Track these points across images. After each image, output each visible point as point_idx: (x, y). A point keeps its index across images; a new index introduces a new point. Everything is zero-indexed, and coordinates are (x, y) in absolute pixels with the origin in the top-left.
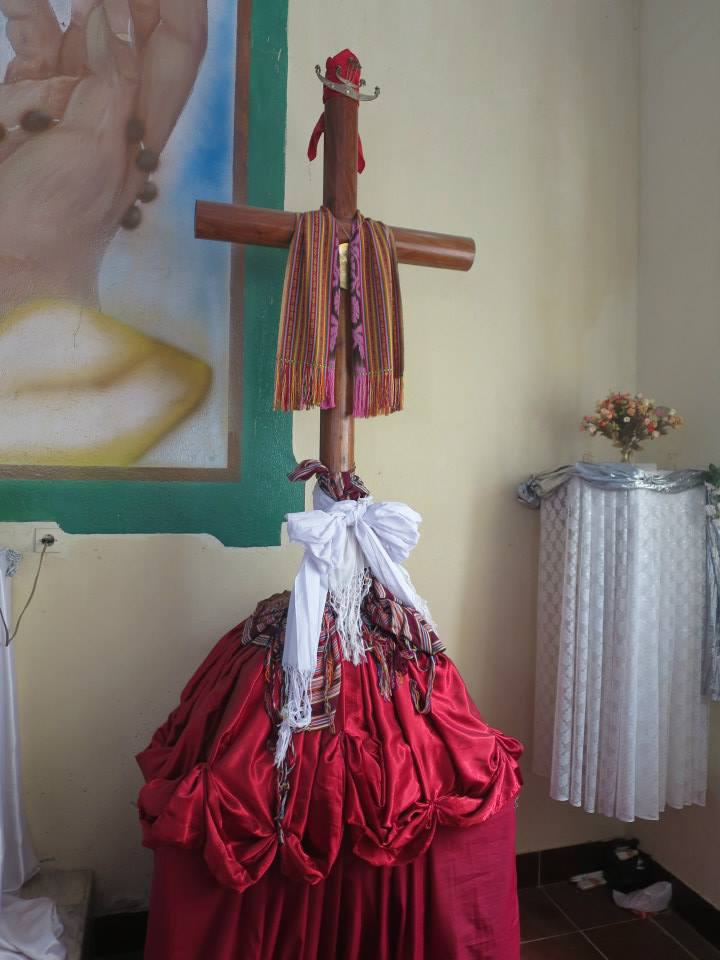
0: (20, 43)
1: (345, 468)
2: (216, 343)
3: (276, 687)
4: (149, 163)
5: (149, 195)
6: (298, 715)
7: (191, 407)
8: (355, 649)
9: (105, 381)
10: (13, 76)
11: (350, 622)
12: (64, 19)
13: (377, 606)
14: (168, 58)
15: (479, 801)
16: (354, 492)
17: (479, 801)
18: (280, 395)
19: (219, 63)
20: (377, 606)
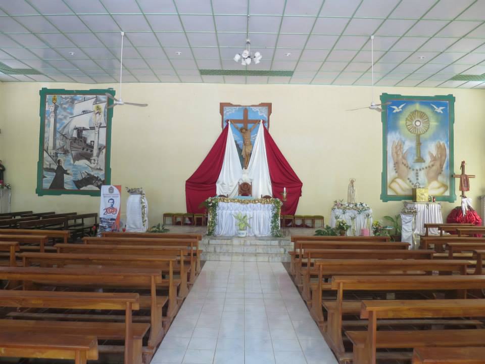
0: (431, 158)
1: (124, 227)
2: (448, 184)
3: (462, 212)
4: (442, 168)
5: (442, 171)
6: (464, 213)
7: (446, 190)
8: (467, 210)
9: (439, 188)
10: (431, 161)
11: (467, 208)
12: (434, 155)
13: (469, 207)
14: (443, 158)
15: (45, 152)
16: (466, 197)
17: (45, 152)
18: (110, 251)
19: (448, 157)
20: (469, 207)
